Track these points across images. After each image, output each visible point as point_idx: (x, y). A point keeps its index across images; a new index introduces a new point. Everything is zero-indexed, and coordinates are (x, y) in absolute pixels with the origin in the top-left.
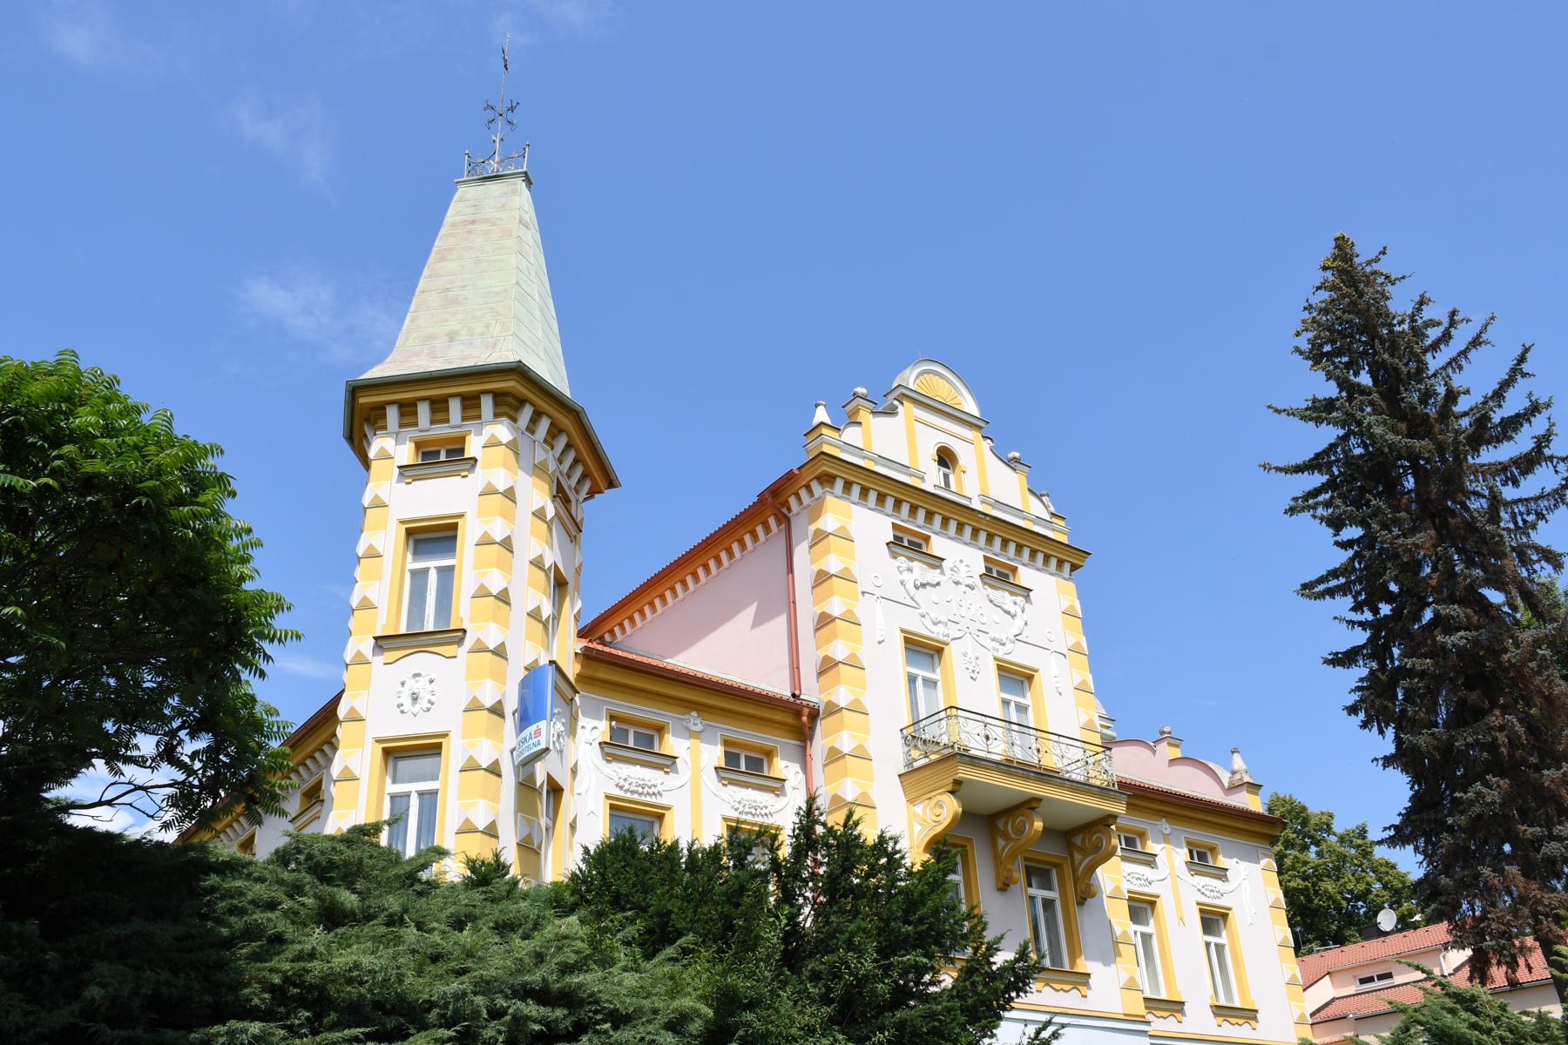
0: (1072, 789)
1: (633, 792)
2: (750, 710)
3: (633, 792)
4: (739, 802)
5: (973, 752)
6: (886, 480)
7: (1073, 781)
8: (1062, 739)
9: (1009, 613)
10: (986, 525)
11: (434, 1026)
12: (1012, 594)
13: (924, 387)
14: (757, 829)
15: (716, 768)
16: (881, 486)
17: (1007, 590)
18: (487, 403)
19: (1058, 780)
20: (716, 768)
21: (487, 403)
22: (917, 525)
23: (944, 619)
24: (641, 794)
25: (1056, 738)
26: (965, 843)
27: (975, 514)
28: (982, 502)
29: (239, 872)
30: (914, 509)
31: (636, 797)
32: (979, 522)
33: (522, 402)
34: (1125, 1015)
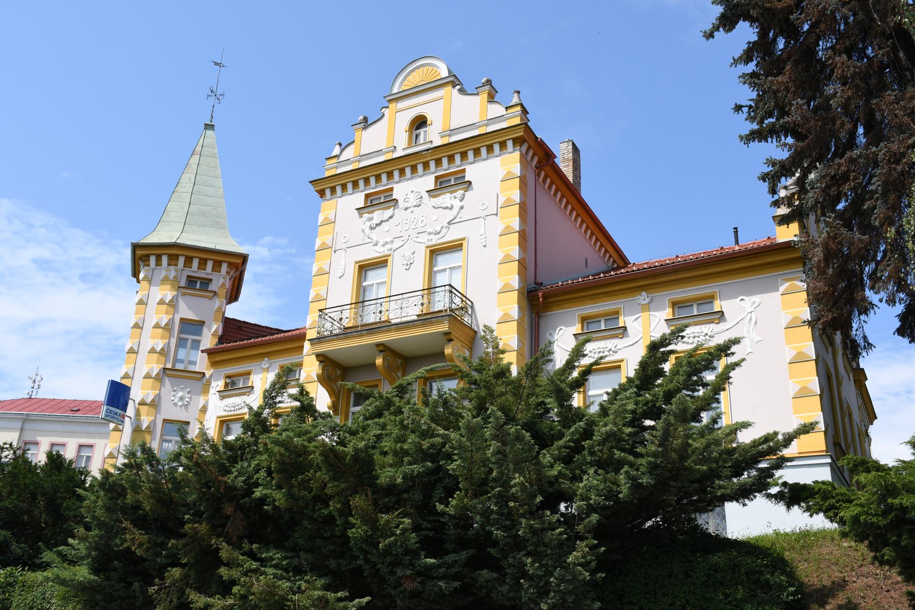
0: (397, 330)
1: (231, 411)
2: (289, 346)
3: (231, 411)
4: (227, 406)
5: (393, 322)
6: (353, 172)
7: (325, 337)
8: (405, 296)
9: (447, 208)
10: (431, 156)
11: (547, 529)
12: (451, 192)
13: (431, 75)
14: (290, 410)
15: (574, 335)
16: (339, 181)
17: (447, 192)
18: (510, 144)
19: (386, 328)
20: (574, 335)
21: (510, 144)
22: (373, 188)
23: (388, 240)
24: (234, 410)
25: (400, 297)
26: (377, 383)
27: (420, 154)
28: (442, 137)
29: (53, 486)
30: (367, 181)
31: (232, 413)
32: (424, 158)
33: (148, 256)
34: (799, 453)
